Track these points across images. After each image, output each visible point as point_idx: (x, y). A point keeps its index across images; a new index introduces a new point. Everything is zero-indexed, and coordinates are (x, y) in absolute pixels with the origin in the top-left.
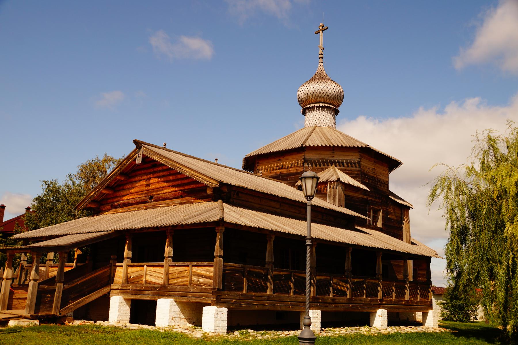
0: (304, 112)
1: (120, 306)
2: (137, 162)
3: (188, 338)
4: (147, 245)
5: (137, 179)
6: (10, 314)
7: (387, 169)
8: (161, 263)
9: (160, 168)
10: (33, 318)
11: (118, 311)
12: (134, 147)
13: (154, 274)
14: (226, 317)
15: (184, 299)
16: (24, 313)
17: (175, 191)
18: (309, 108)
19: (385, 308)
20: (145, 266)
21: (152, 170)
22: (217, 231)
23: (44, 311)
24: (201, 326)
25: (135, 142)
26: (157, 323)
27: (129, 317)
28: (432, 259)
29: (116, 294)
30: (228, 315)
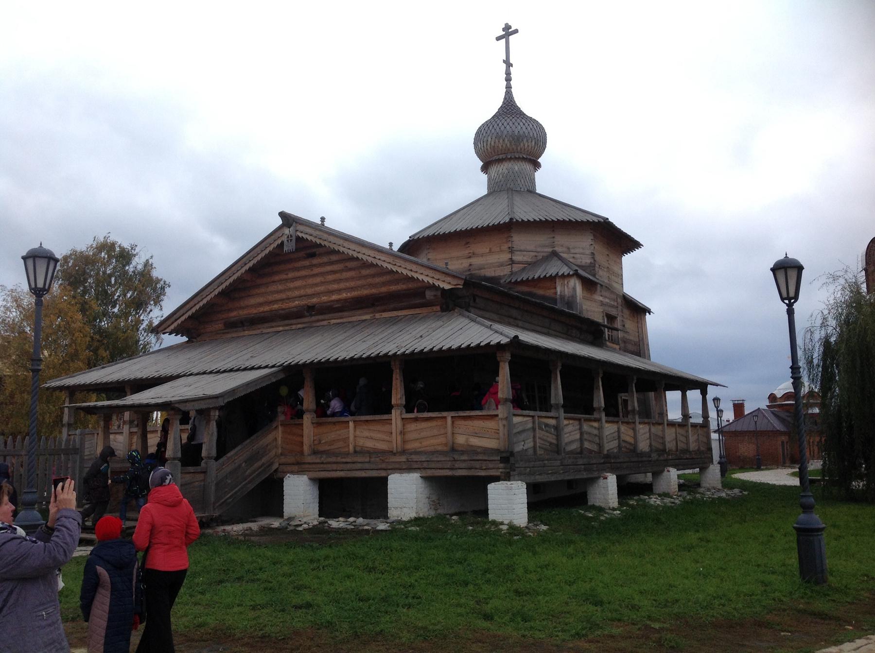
2: (286, 249)
4: (358, 386)
8: (386, 417)
9: (325, 259)
11: (300, 497)
12: (279, 222)
13: (362, 435)
15: (429, 473)
17: (231, 310)
20: (351, 424)
21: (307, 263)
22: (498, 359)
25: (282, 215)
28: (709, 387)
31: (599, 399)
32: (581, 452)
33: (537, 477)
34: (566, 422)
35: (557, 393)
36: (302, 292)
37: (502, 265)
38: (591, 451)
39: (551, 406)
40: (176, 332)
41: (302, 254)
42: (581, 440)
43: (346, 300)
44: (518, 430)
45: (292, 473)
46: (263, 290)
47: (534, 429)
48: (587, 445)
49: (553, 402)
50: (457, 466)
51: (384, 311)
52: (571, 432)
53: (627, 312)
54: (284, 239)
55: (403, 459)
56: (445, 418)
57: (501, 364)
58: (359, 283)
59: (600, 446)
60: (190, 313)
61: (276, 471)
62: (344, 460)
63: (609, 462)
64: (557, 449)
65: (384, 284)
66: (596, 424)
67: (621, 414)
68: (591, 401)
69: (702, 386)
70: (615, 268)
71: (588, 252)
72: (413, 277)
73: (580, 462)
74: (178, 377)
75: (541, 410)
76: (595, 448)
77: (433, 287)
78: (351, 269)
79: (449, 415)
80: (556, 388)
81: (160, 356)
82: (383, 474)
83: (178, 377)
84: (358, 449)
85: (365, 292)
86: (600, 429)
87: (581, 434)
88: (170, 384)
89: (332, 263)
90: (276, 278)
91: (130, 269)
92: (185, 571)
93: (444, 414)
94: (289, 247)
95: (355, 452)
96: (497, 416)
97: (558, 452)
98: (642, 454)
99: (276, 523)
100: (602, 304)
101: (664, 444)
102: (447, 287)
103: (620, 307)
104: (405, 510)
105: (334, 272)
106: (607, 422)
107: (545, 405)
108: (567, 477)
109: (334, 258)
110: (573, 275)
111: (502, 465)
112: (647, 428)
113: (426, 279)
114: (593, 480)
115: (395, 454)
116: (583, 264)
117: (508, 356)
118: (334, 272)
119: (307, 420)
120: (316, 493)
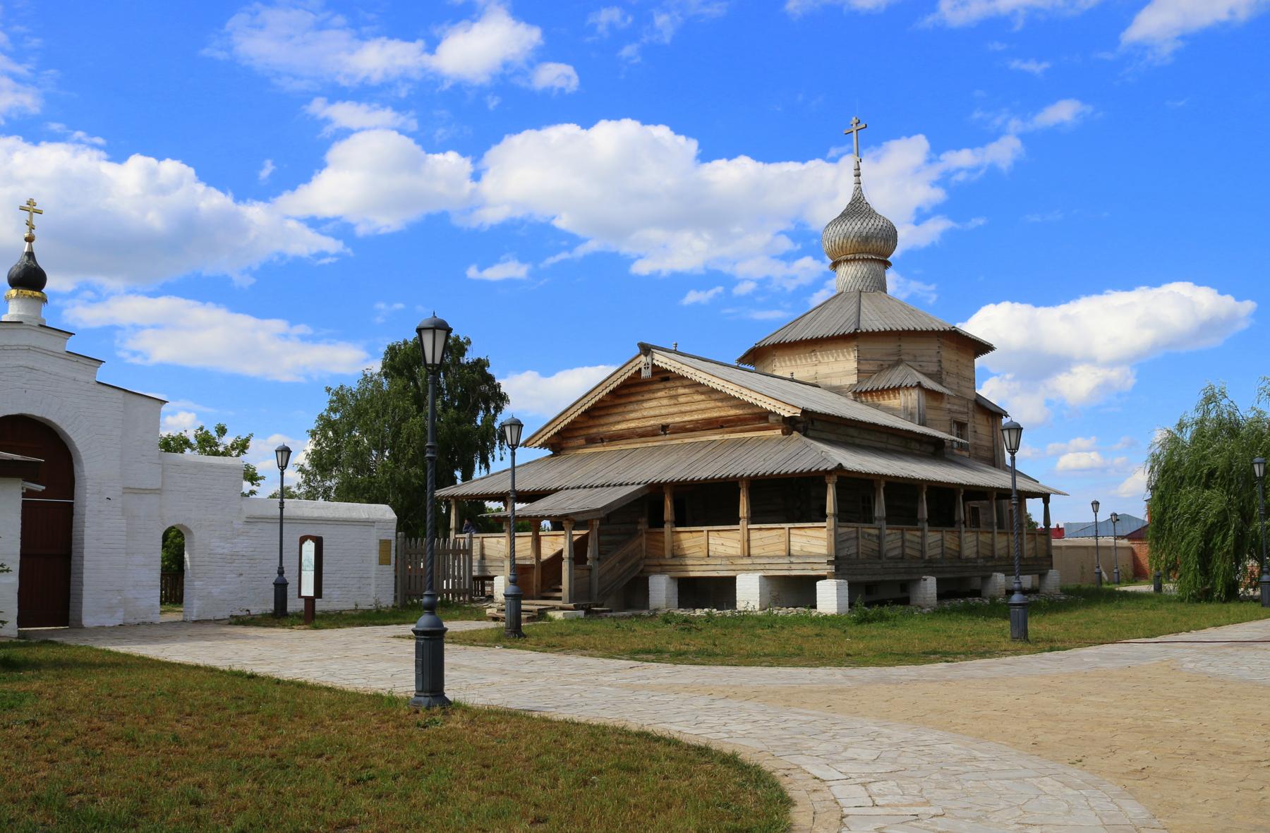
2: (643, 375)
9: (678, 383)
12: (638, 351)
28: (1052, 497)
32: (902, 558)
34: (888, 532)
35: (880, 509)
36: (657, 412)
38: (913, 557)
40: (543, 446)
41: (657, 378)
42: (903, 545)
43: (697, 421)
46: (620, 410)
47: (857, 538)
48: (908, 551)
51: (732, 432)
52: (893, 539)
54: (642, 365)
59: (922, 552)
61: (642, 571)
63: (930, 566)
64: (879, 555)
66: (919, 533)
70: (967, 373)
71: (935, 359)
73: (901, 565)
74: (556, 490)
76: (917, 554)
79: (787, 526)
81: (532, 470)
83: (556, 490)
85: (715, 414)
86: (923, 537)
87: (903, 542)
88: (549, 498)
90: (633, 399)
91: (464, 360)
93: (783, 525)
94: (646, 374)
97: (880, 558)
98: (968, 560)
100: (950, 411)
101: (993, 551)
102: (787, 415)
103: (971, 414)
107: (868, 518)
109: (686, 382)
112: (1005, 538)
114: (917, 581)
117: (834, 478)
120: (676, 589)
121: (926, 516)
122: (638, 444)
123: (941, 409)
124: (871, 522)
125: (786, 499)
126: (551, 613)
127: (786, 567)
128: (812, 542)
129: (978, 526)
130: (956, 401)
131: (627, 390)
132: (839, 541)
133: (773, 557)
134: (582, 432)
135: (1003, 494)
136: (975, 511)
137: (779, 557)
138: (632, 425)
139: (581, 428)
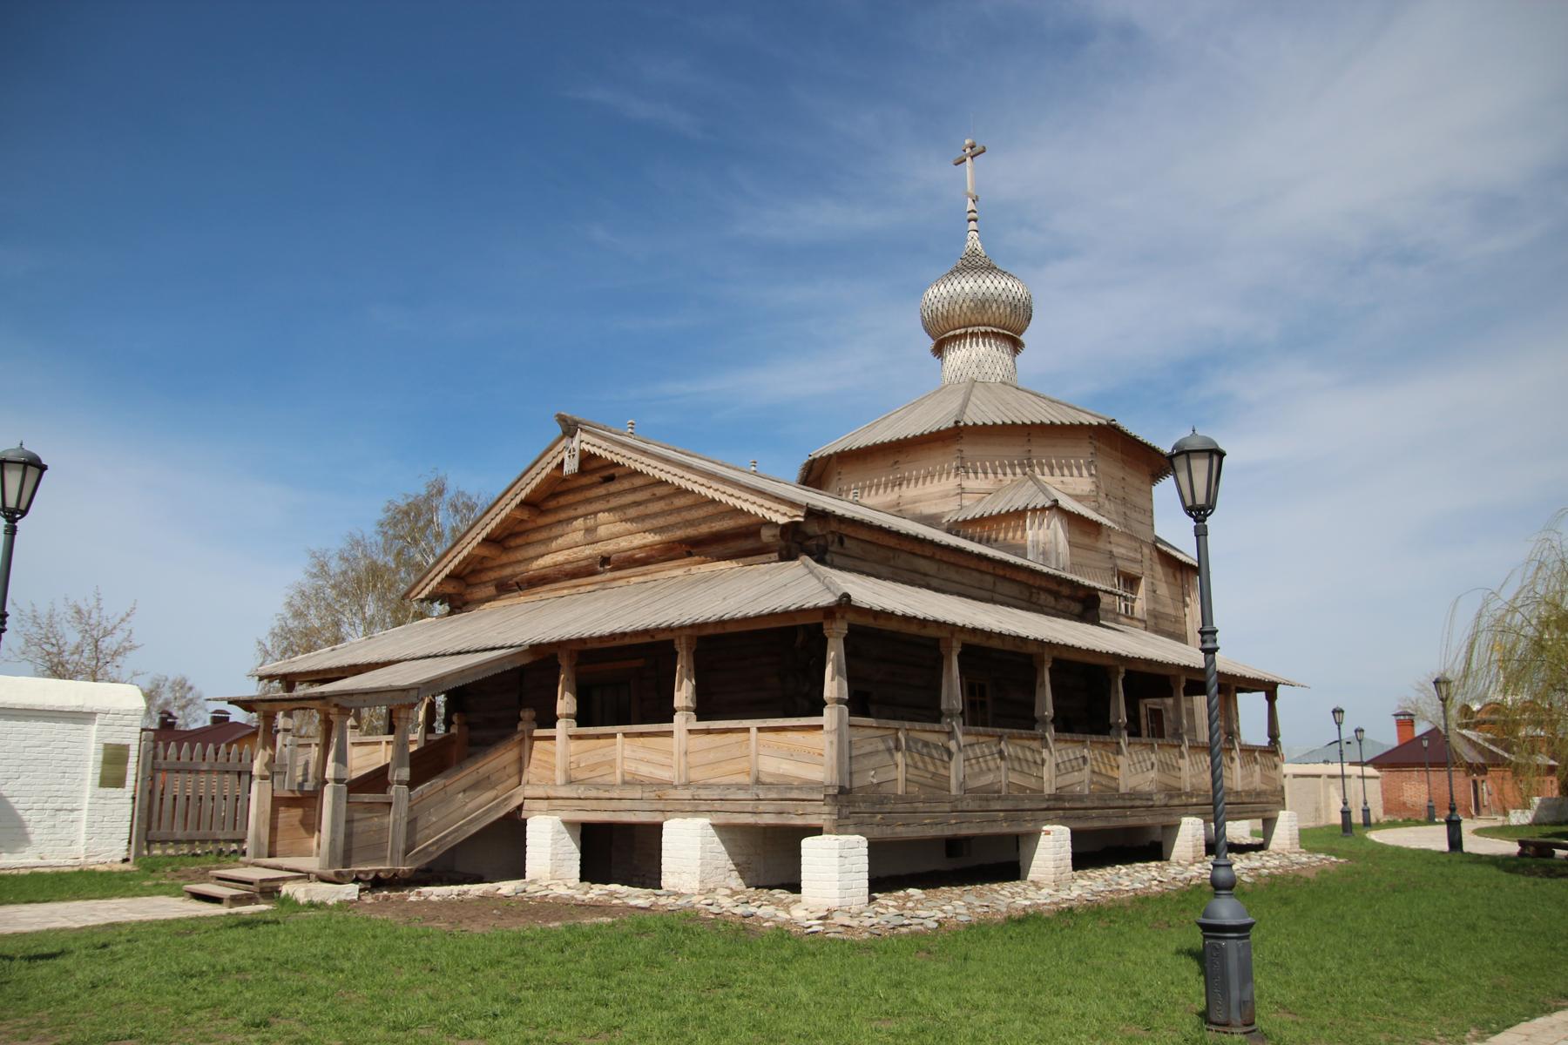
0: (939, 349)
1: (555, 841)
2: (566, 469)
3: (899, 937)
5: (563, 515)
6: (280, 869)
7: (1148, 479)
8: (665, 727)
9: (626, 484)
10: (338, 879)
11: (550, 854)
12: (558, 431)
14: (862, 863)
15: (722, 819)
16: (312, 864)
17: (502, 566)
18: (955, 338)
19: (1196, 815)
21: (601, 491)
23: (365, 861)
24: (795, 887)
25: (562, 419)
26: (667, 880)
27: (578, 868)
28: (1280, 689)
29: (682, 812)
30: (870, 856)
31: (1119, 711)
33: (899, 829)
37: (947, 496)
39: (1110, 727)
44: (862, 751)
45: (541, 811)
46: (544, 535)
49: (944, 706)
50: (761, 808)
53: (1159, 570)
55: (687, 794)
56: (747, 730)
57: (831, 642)
58: (672, 519)
60: (447, 571)
62: (607, 795)
63: (1059, 807)
65: (705, 519)
67: (1144, 732)
68: (1032, 707)
69: (1270, 689)
70: (1139, 500)
72: (713, 500)
74: (399, 661)
75: (993, 726)
77: (770, 523)
78: (662, 498)
80: (950, 686)
82: (656, 818)
83: (399, 661)
84: (628, 778)
89: (634, 490)
92: (1179, 952)
95: (625, 783)
96: (821, 727)
99: (637, 897)
102: (782, 520)
104: (684, 876)
105: (637, 504)
106: (1056, 740)
107: (929, 711)
108: (948, 832)
109: (638, 482)
110: (1050, 508)
111: (826, 809)
113: (760, 512)
115: (676, 787)
116: (1078, 492)
118: (637, 504)
119: (563, 728)
121: (1049, 712)
122: (564, 589)
123: (1096, 550)
124: (937, 720)
125: (755, 671)
126: (286, 889)
127: (750, 806)
128: (796, 755)
129: (1162, 736)
130: (1122, 541)
131: (548, 502)
132: (849, 757)
133: (728, 786)
134: (493, 575)
135: (1195, 681)
136: (1156, 715)
137: (740, 787)
138: (560, 557)
139: (491, 569)
